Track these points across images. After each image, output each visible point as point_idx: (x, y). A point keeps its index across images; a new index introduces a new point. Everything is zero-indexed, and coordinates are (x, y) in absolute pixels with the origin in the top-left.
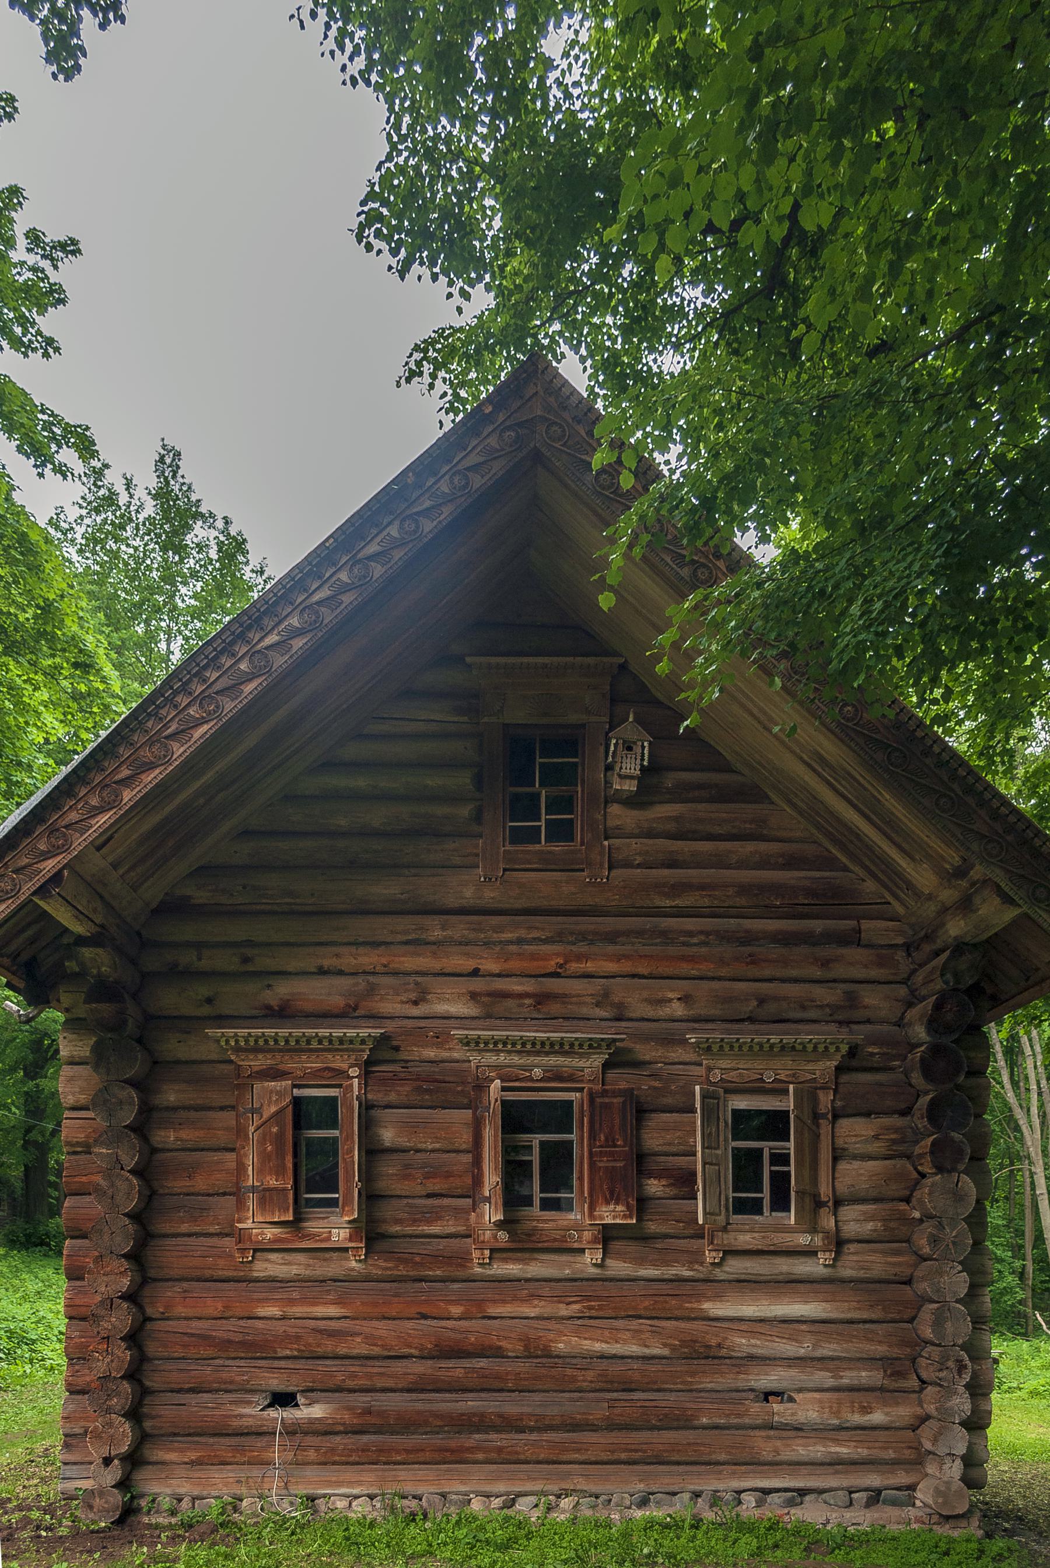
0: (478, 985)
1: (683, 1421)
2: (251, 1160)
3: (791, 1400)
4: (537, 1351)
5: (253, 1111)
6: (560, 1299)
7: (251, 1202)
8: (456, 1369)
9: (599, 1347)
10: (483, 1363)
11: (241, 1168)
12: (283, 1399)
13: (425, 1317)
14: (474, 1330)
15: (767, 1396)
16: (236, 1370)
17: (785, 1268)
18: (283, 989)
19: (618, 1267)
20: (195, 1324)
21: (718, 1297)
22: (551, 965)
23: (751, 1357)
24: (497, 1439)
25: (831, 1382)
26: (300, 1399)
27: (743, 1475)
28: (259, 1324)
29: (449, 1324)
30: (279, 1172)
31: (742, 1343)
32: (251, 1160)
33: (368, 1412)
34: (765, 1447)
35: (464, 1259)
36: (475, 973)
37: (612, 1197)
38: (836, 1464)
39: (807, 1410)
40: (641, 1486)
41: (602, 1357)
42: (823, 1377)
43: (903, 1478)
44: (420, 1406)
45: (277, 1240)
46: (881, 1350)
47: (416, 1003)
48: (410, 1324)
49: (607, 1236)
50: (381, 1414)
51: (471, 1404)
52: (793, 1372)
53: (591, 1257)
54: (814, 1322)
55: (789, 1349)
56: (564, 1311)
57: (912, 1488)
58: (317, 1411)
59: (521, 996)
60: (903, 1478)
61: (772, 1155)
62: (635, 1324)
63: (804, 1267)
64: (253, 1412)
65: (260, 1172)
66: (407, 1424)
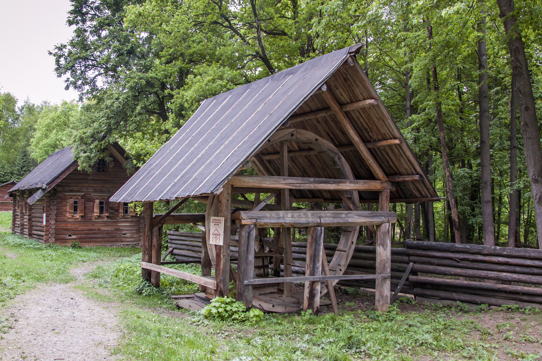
1: (115, 237)
2: (68, 208)
4: (99, 230)
8: (91, 232)
12: (70, 236)
14: (92, 227)
15: (124, 234)
18: (72, 188)
19: (109, 220)
31: (121, 228)
32: (68, 208)
34: (124, 239)
35: (92, 219)
39: (128, 235)
42: (130, 232)
49: (108, 217)
51: (92, 236)
55: (126, 229)
63: (128, 220)
64: (67, 237)
66: (85, 238)
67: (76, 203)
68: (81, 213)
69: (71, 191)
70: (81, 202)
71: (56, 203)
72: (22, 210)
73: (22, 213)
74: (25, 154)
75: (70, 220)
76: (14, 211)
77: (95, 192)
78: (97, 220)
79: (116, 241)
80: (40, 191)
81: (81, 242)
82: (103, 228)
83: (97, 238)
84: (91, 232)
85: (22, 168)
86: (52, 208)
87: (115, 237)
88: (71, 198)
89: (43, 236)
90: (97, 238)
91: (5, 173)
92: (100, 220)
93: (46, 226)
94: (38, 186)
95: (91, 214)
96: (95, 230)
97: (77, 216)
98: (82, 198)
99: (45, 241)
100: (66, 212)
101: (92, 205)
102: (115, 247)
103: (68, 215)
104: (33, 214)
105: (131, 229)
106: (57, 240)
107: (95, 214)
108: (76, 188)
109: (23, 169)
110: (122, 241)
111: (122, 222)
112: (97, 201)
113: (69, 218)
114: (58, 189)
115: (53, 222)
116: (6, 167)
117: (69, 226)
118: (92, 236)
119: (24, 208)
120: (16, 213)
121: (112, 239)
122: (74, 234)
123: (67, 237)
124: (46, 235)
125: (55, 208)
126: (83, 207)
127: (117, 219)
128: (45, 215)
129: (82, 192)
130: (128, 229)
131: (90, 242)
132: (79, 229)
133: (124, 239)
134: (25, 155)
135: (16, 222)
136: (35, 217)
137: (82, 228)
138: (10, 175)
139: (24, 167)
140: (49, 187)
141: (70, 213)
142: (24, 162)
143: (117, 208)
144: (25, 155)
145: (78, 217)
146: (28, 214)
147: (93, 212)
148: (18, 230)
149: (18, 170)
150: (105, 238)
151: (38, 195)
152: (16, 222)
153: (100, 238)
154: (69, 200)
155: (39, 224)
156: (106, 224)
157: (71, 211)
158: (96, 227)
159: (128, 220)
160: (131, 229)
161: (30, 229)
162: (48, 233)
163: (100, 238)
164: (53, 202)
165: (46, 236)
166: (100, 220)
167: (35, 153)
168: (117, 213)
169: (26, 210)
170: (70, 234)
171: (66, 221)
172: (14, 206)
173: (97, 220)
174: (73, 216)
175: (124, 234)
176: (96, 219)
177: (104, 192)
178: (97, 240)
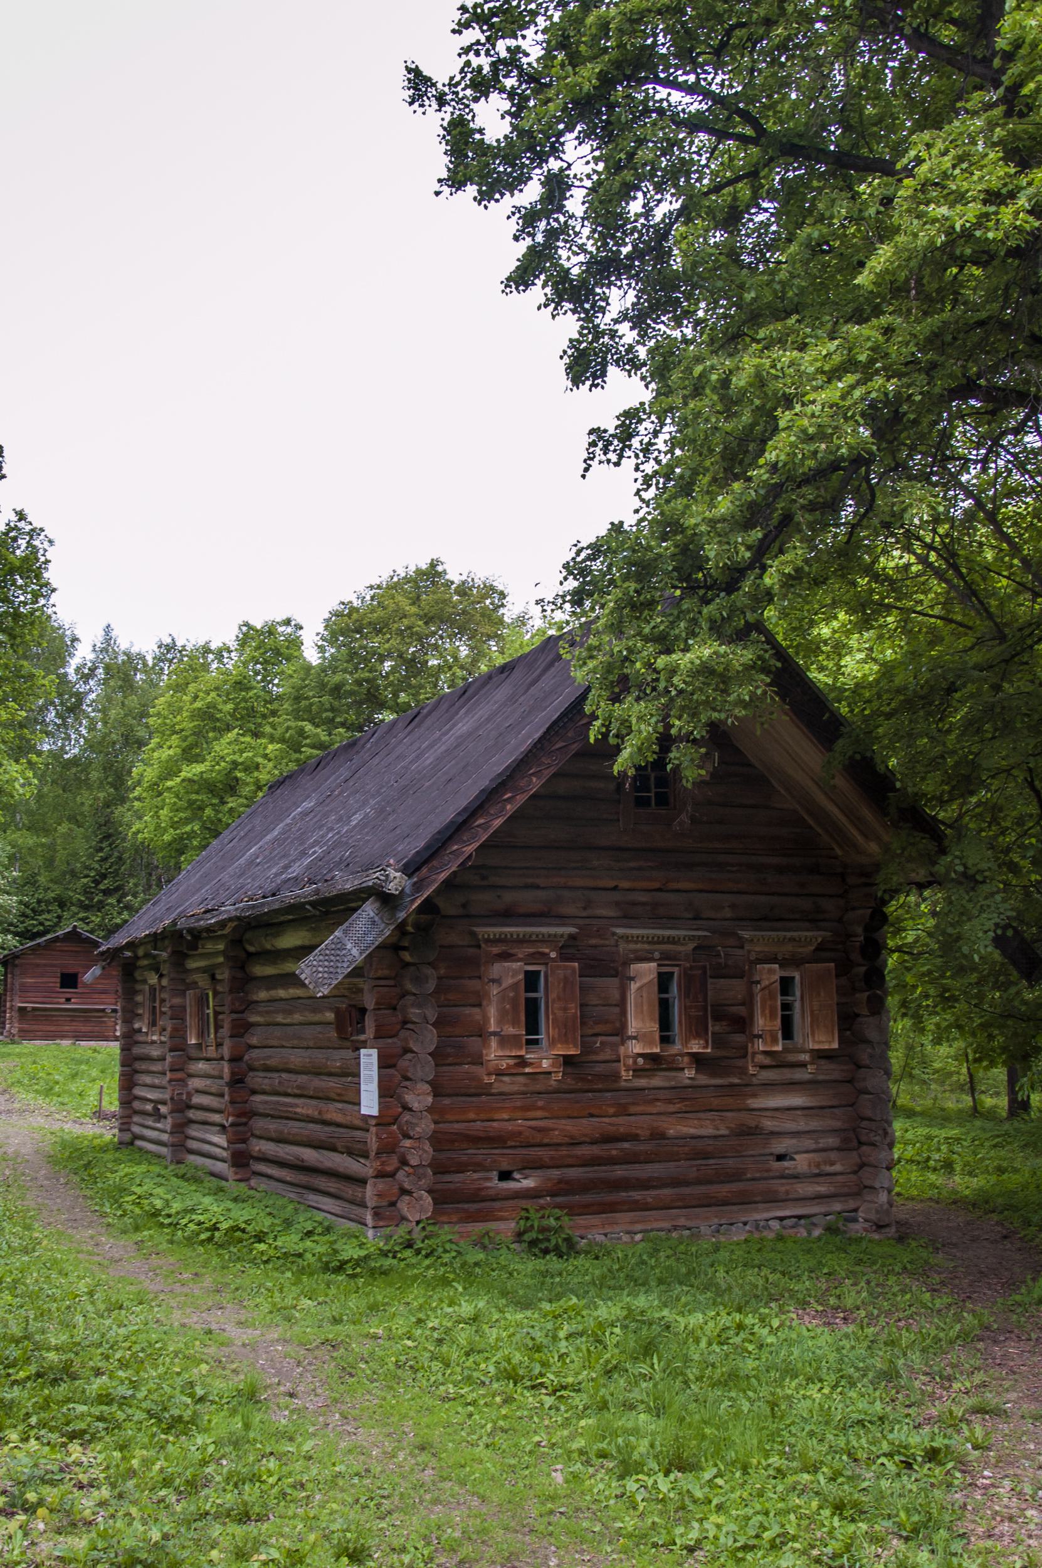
0: (617, 896)
1: (736, 1176)
2: (492, 1012)
3: (793, 1159)
4: (658, 1135)
5: (493, 981)
6: (669, 1101)
7: (494, 1042)
8: (614, 1149)
9: (692, 1131)
10: (626, 1145)
11: (486, 1019)
12: (505, 1176)
13: (592, 1115)
14: (622, 1124)
15: (780, 1158)
16: (478, 1153)
17: (789, 1076)
18: (509, 897)
19: (703, 1080)
20: (456, 1126)
21: (754, 1095)
22: (657, 885)
23: (772, 1133)
24: (636, 1195)
25: (813, 1146)
26: (517, 1175)
27: (768, 1210)
28: (495, 1124)
29: (606, 1120)
30: (515, 1023)
31: (768, 1124)
32: (492, 1012)
33: (560, 1181)
34: (781, 1186)
35: (617, 1076)
36: (615, 888)
37: (698, 1036)
38: (819, 1198)
39: (801, 1163)
40: (716, 1221)
41: (693, 1137)
42: (809, 1143)
43: (852, 1204)
44: (591, 1175)
45: (509, 1067)
46: (837, 1124)
47: (585, 908)
48: (584, 1121)
49: (698, 1060)
50: (567, 1182)
51: (620, 1171)
52: (794, 1141)
53: (690, 1073)
54: (804, 1108)
55: (790, 1126)
56: (671, 1108)
57: (856, 1210)
58: (529, 1183)
59: (644, 904)
60: (852, 1204)
61: (649, 805)
62: (709, 1115)
63: (799, 1075)
64: (495, 1184)
65: (500, 1021)
66: (585, 1187)
67: (531, 981)
68: (564, 1039)
69: (508, 915)
70: (558, 975)
71: (431, 986)
72: (179, 1034)
73: (178, 1046)
74: (108, 833)
75: (508, 1084)
76: (129, 1041)
77: (628, 916)
78: (642, 1082)
79: (745, 1200)
80: (369, 909)
81: (573, 1211)
82: (675, 1128)
83: (645, 1184)
84: (614, 1149)
85: (97, 883)
86: (414, 1013)
87: (736, 1176)
88: (505, 956)
89: (362, 1182)
90: (645, 1184)
91: (39, 901)
92: (657, 1082)
93: (382, 1121)
94: (347, 883)
95: (615, 1047)
96: (634, 1138)
97: (544, 1060)
98: (564, 957)
99: (377, 1215)
100: (482, 1033)
101: (616, 995)
102: (738, 1235)
103: (494, 1053)
104: (255, 1053)
105: (814, 1124)
106: (443, 1199)
107: (636, 1048)
108: (528, 900)
109: (101, 887)
110: (772, 1199)
111: (770, 1087)
112: (646, 972)
113: (500, 1073)
114: (447, 907)
115: (419, 1098)
116: (42, 880)
117: (505, 1122)
118: (620, 1171)
119: (191, 1021)
120: (137, 1050)
121: (723, 1190)
122: (529, 1166)
123: (495, 1184)
124: (380, 1175)
125: (432, 1014)
126: (574, 1009)
127: (743, 1071)
128: (369, 1060)
129: (562, 919)
130: (802, 1125)
131: (611, 1208)
132: (556, 1137)
133: (781, 1186)
134: (107, 837)
135: (138, 1091)
136: (268, 1069)
137: (570, 1126)
138: (54, 907)
139: (104, 876)
140: (418, 887)
141: (505, 1041)
142: (104, 860)
143: (742, 1010)
144: (107, 837)
145: (545, 1064)
146: (226, 1051)
147: (620, 1032)
148: (159, 1131)
149: (86, 891)
150: (687, 1183)
151: (357, 938)
152: (138, 1091)
153: (661, 1183)
154: (497, 969)
155: (333, 1112)
156: (688, 1100)
157: (510, 1030)
158: (639, 1123)
159: (799, 1075)
160: (814, 1124)
161: (241, 1128)
162: (393, 1163)
163: (661, 1183)
164: (418, 980)
165: (381, 1185)
166: (657, 1082)
167: (146, 823)
168: (739, 1038)
169: (202, 1034)
170: (505, 1166)
171: (484, 1091)
172: (130, 1016)
173: (642, 1082)
174: (522, 1062)
175: (780, 1158)
176: (638, 1072)
177: (672, 920)
178: (649, 1195)
